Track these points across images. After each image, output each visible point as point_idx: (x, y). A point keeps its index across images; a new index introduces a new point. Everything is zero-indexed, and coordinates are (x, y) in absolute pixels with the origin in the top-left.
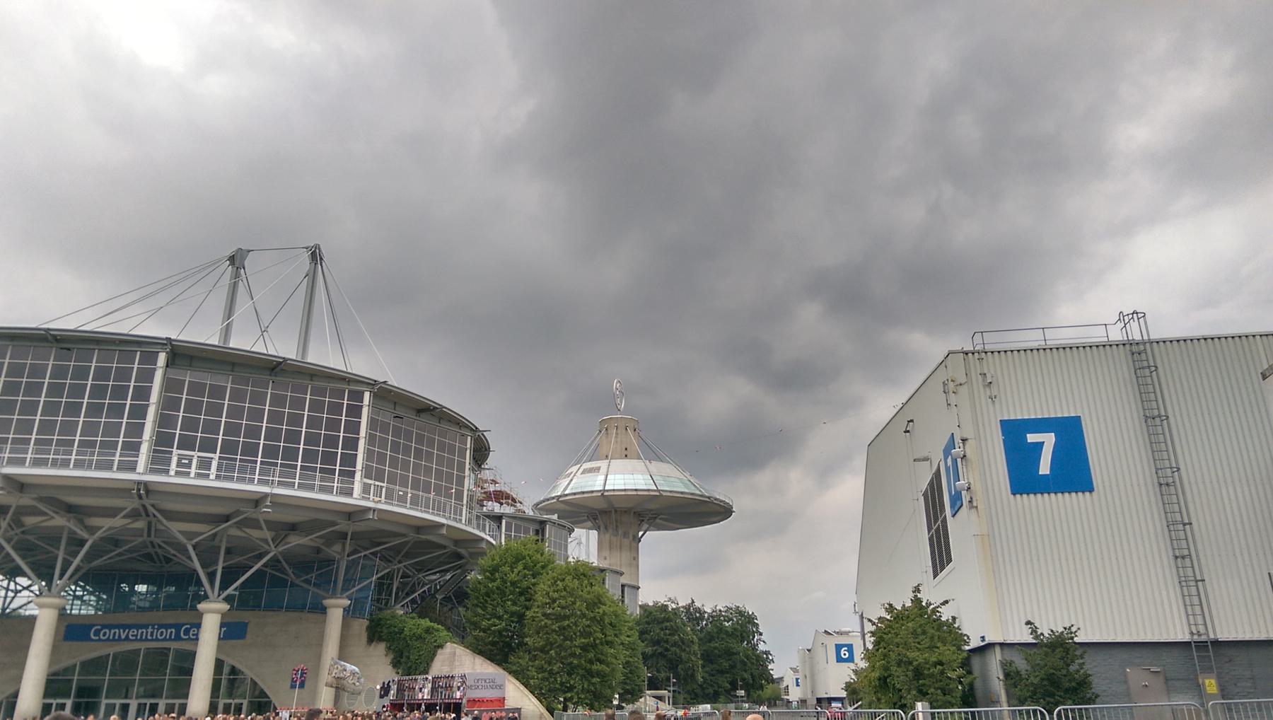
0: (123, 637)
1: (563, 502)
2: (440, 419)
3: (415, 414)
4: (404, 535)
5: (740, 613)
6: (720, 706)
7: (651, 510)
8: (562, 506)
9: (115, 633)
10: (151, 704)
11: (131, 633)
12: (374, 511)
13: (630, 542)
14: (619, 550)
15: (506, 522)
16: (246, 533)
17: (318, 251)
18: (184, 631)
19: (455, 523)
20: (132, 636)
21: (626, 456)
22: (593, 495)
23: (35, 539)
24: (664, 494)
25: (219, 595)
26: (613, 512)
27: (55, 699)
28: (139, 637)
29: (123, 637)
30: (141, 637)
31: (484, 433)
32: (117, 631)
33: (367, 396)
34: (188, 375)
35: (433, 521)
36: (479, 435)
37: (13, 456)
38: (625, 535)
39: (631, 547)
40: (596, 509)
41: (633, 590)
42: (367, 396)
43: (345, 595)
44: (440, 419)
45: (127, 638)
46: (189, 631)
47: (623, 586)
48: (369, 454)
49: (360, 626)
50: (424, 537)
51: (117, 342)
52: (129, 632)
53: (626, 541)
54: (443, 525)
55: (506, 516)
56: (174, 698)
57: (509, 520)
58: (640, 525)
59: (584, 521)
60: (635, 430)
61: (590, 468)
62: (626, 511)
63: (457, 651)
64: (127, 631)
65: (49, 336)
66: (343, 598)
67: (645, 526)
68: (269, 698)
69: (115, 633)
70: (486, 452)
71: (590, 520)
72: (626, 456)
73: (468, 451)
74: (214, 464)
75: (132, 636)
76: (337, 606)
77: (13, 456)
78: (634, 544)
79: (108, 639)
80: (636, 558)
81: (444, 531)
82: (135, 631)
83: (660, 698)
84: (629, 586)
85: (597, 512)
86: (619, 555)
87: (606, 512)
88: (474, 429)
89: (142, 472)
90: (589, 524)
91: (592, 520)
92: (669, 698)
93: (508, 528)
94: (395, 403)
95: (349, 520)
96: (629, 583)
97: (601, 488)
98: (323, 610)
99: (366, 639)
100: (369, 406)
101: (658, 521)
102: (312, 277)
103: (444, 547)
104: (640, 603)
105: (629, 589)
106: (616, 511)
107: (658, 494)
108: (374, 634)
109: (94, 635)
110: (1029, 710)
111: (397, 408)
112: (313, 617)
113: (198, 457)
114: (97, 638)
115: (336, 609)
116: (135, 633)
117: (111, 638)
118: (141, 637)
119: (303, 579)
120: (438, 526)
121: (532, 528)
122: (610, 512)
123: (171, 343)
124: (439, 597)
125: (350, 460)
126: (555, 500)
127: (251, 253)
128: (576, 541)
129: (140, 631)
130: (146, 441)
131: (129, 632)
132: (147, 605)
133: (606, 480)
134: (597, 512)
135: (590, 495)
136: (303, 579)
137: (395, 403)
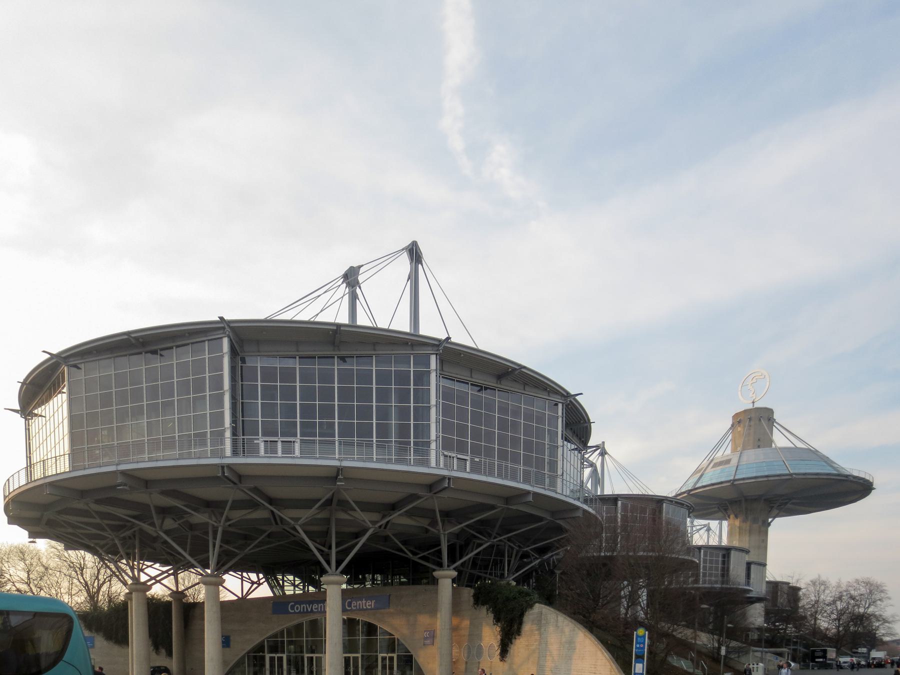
0: (309, 610)
2: (525, 384)
3: (495, 381)
4: (493, 507)
5: (868, 583)
6: (523, 589)
9: (304, 607)
10: (278, 657)
11: (314, 607)
12: (449, 479)
16: (351, 516)
17: (414, 248)
18: (348, 603)
20: (315, 609)
22: (723, 485)
23: (200, 533)
24: (797, 477)
25: (337, 568)
27: (276, 654)
28: (319, 610)
29: (309, 610)
30: (321, 610)
31: (577, 398)
32: (305, 605)
33: (433, 359)
34: (259, 360)
36: (570, 401)
37: (469, 444)
38: (755, 520)
41: (759, 567)
42: (433, 359)
43: (452, 567)
44: (525, 384)
45: (312, 611)
46: (351, 604)
47: (749, 565)
48: (446, 427)
49: (468, 593)
51: (187, 335)
52: (312, 606)
54: (528, 492)
55: (621, 497)
56: (350, 653)
58: (770, 511)
59: (715, 512)
61: (720, 462)
62: (756, 499)
63: (544, 610)
64: (311, 605)
65: (131, 338)
66: (450, 570)
67: (775, 512)
68: (410, 653)
69: (304, 607)
70: (586, 425)
73: (560, 420)
74: (297, 446)
75: (315, 609)
76: (446, 577)
77: (469, 444)
79: (300, 612)
80: (765, 541)
81: (530, 498)
82: (355, 603)
83: (780, 655)
84: (756, 563)
85: (727, 502)
86: (747, 539)
87: (736, 502)
88: (565, 394)
89: (228, 457)
90: (720, 514)
91: (723, 510)
92: (788, 654)
93: (705, 555)
94: (471, 369)
95: (430, 492)
97: (732, 478)
98: (435, 581)
99: (386, 587)
100: (436, 370)
101: (789, 506)
102: (414, 278)
103: (540, 519)
104: (767, 580)
105: (737, 553)
106: (746, 500)
107: (790, 477)
108: (479, 600)
109: (291, 610)
110: (349, 657)
111: (473, 375)
112: (431, 587)
113: (282, 442)
114: (350, 608)
115: (446, 578)
116: (317, 607)
117: (302, 611)
118: (321, 610)
119: (419, 556)
120: (525, 493)
122: (740, 501)
123: (228, 326)
124: (558, 572)
125: (422, 431)
126: (686, 495)
127: (361, 268)
128: (598, 451)
129: (320, 605)
130: (227, 428)
131: (312, 606)
134: (727, 502)
135: (720, 486)
136: (419, 556)
137: (471, 369)
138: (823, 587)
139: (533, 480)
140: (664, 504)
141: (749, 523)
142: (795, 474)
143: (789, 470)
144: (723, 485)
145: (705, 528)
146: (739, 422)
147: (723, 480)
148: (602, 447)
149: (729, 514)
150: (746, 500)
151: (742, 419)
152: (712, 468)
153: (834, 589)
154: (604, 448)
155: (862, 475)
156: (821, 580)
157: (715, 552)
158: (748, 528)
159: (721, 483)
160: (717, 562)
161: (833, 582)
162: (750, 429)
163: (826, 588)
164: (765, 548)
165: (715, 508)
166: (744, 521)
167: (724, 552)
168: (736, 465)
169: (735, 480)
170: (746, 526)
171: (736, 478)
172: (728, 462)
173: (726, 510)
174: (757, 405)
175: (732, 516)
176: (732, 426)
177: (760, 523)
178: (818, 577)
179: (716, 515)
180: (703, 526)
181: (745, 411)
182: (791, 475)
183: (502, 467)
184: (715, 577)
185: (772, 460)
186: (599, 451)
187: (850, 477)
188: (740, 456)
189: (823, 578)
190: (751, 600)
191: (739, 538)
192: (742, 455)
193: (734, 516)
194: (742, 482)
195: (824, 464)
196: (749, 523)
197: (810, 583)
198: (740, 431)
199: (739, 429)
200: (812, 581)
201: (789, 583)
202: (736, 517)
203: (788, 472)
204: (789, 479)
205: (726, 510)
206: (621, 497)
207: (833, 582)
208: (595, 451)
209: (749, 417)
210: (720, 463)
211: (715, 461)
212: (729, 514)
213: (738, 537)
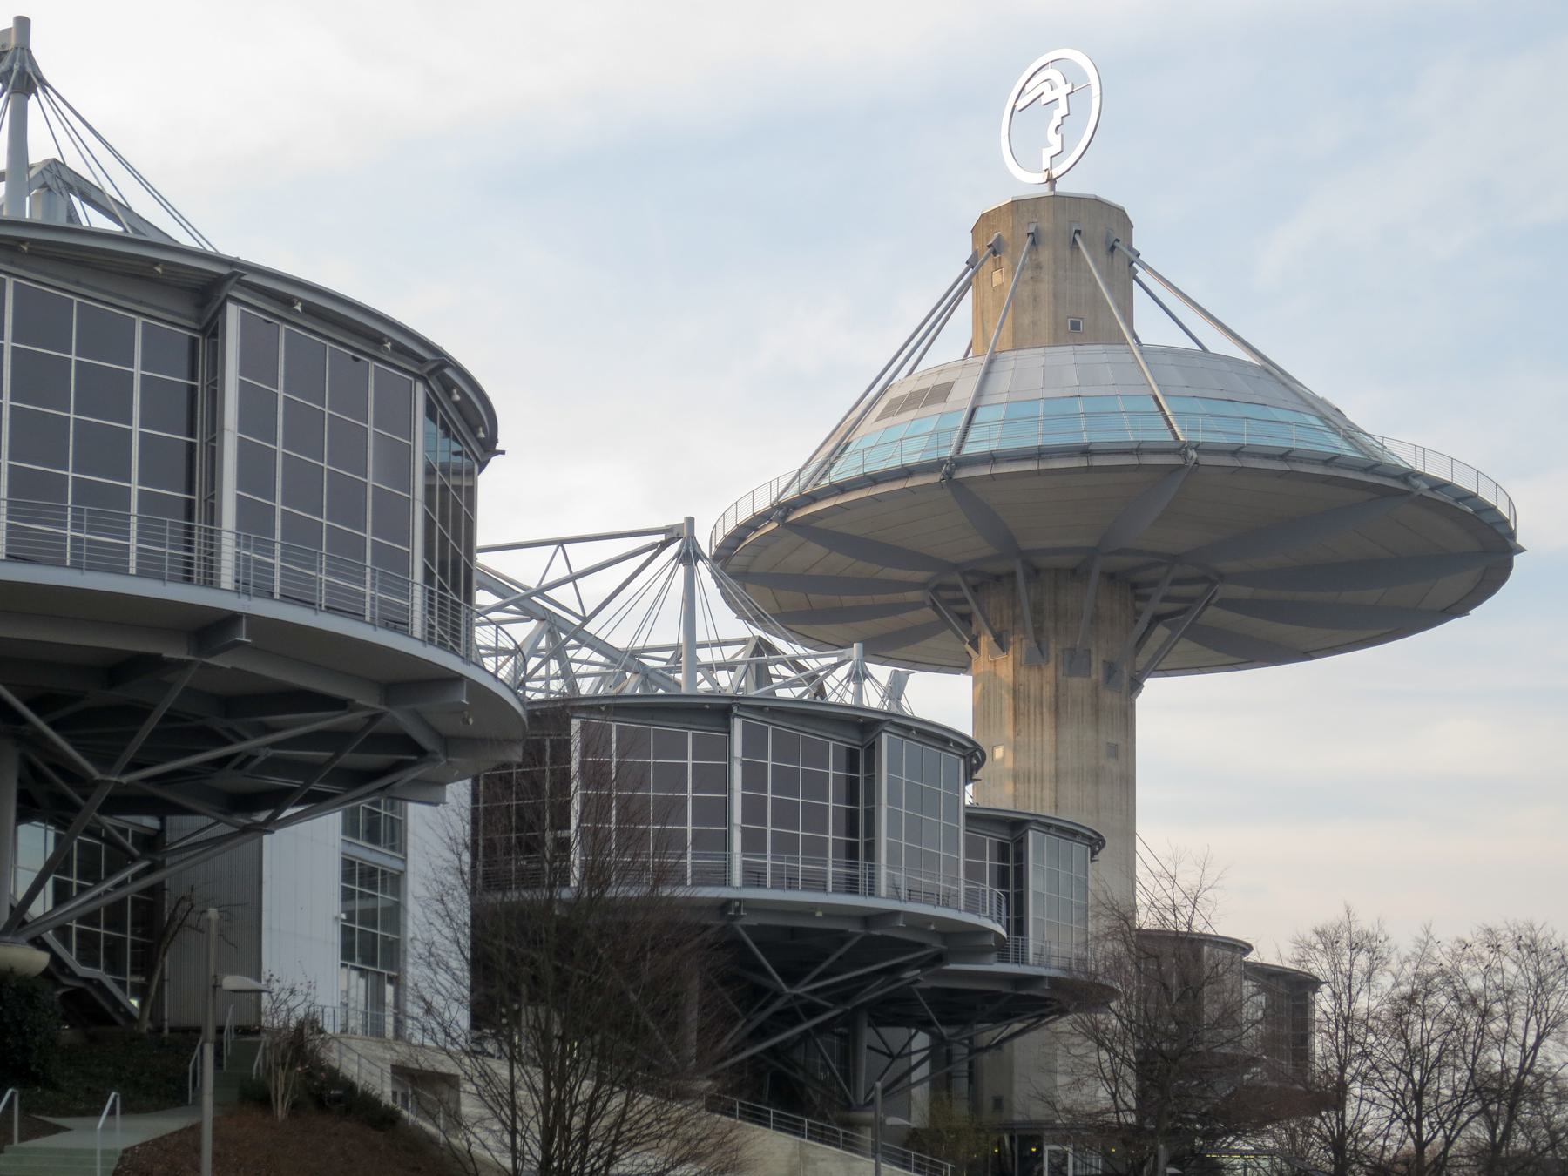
1: (802, 527)
7: (1174, 559)
8: (811, 557)
13: (1095, 689)
14: (1048, 718)
15: (745, 726)
19: (990, 921)
21: (1075, 326)
22: (910, 483)
24: (1206, 460)
26: (1020, 577)
35: (964, 923)
38: (1075, 662)
39: (1097, 710)
40: (955, 567)
41: (1064, 843)
50: (877, 933)
53: (1079, 686)
55: (741, 707)
57: (758, 720)
60: (1113, 248)
71: (950, 626)
72: (1075, 326)
78: (1109, 698)
84: (1047, 826)
85: (956, 578)
86: (1048, 735)
90: (945, 642)
93: (754, 742)
96: (1047, 811)
97: (947, 453)
105: (1049, 840)
106: (1034, 573)
121: (834, 747)
128: (674, 548)
132: (519, 1146)
133: (1144, 634)
138: (1362, 960)
139: (321, 591)
140: (884, 736)
141: (1049, 672)
142: (1197, 447)
143: (1174, 434)
144: (910, 483)
145: (674, 548)
146: (995, 250)
147: (912, 460)
148: (685, 533)
149: (974, 632)
150: (1034, 573)
151: (1006, 235)
152: (878, 419)
153: (1407, 966)
154: (693, 538)
155: (1465, 482)
156: (1355, 929)
157: (801, 734)
158: (1048, 692)
159: (906, 472)
160: (816, 786)
161: (1401, 941)
162: (1035, 280)
163: (1378, 960)
164: (1127, 782)
165: (917, 605)
166: (1036, 657)
167: (852, 740)
168: (968, 405)
169: (958, 462)
170: (1042, 681)
171: (968, 450)
172: (939, 393)
173: (966, 619)
174: (1062, 187)
175: (986, 640)
176: (971, 263)
177: (1097, 672)
178: (1343, 915)
179: (932, 642)
180: (661, 538)
181: (1016, 206)
182: (1180, 449)
183: (171, 539)
184: (310, 561)
185: (1112, 391)
186: (849, 665)
187: (1417, 482)
188: (987, 373)
189: (1365, 922)
190: (1032, 992)
191: (1017, 733)
192: (996, 366)
193: (992, 639)
194: (985, 471)
195: (1315, 421)
196: (1049, 672)
197: (1314, 939)
198: (1001, 286)
199: (997, 278)
200: (1321, 934)
201: (1247, 948)
202: (1001, 642)
203: (1169, 437)
204: (1179, 467)
205: (966, 619)
206: (741, 707)
207: (1401, 941)
208: (664, 545)
209: (1032, 229)
210: (915, 400)
211: (893, 394)
212: (974, 632)
213: (1009, 732)
